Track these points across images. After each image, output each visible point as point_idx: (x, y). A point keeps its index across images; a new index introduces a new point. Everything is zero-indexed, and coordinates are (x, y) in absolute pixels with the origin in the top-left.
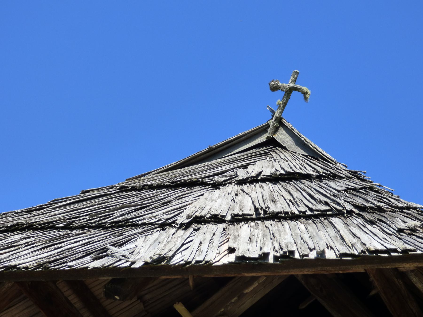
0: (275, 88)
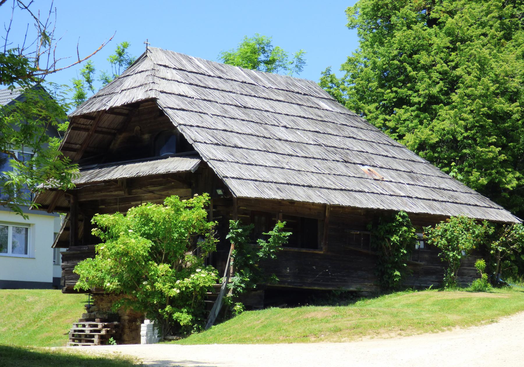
0: (144, 43)
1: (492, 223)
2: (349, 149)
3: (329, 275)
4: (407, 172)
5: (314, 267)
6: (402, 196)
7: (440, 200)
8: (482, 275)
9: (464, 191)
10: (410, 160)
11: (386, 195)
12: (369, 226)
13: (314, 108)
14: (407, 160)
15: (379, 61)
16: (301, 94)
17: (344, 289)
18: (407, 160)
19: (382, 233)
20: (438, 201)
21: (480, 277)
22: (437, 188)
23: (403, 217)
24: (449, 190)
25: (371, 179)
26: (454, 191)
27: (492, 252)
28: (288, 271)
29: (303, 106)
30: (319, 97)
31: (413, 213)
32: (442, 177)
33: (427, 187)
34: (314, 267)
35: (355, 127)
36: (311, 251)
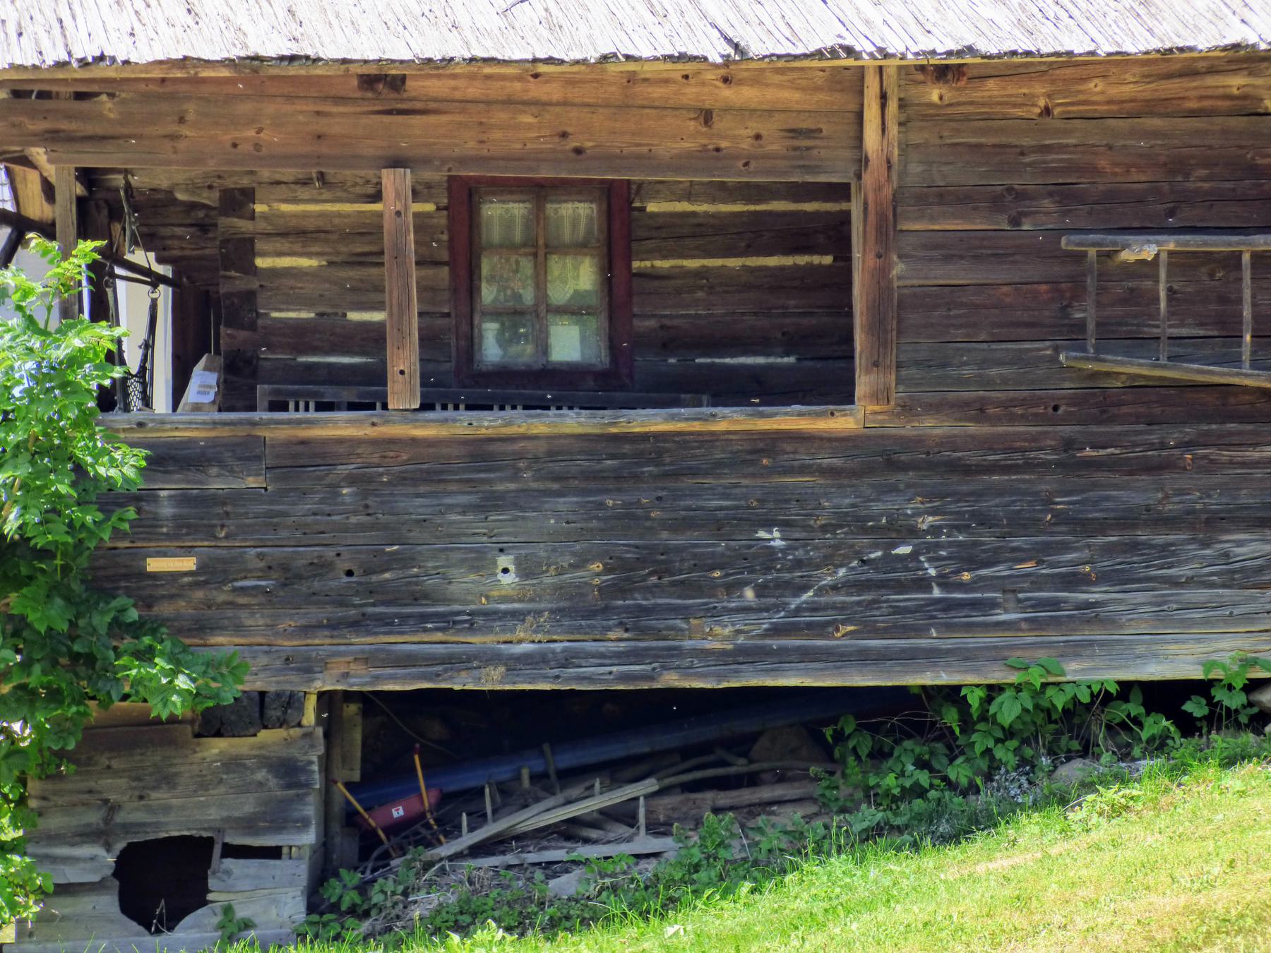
3: (923, 584)
28: (509, 579)
34: (775, 537)
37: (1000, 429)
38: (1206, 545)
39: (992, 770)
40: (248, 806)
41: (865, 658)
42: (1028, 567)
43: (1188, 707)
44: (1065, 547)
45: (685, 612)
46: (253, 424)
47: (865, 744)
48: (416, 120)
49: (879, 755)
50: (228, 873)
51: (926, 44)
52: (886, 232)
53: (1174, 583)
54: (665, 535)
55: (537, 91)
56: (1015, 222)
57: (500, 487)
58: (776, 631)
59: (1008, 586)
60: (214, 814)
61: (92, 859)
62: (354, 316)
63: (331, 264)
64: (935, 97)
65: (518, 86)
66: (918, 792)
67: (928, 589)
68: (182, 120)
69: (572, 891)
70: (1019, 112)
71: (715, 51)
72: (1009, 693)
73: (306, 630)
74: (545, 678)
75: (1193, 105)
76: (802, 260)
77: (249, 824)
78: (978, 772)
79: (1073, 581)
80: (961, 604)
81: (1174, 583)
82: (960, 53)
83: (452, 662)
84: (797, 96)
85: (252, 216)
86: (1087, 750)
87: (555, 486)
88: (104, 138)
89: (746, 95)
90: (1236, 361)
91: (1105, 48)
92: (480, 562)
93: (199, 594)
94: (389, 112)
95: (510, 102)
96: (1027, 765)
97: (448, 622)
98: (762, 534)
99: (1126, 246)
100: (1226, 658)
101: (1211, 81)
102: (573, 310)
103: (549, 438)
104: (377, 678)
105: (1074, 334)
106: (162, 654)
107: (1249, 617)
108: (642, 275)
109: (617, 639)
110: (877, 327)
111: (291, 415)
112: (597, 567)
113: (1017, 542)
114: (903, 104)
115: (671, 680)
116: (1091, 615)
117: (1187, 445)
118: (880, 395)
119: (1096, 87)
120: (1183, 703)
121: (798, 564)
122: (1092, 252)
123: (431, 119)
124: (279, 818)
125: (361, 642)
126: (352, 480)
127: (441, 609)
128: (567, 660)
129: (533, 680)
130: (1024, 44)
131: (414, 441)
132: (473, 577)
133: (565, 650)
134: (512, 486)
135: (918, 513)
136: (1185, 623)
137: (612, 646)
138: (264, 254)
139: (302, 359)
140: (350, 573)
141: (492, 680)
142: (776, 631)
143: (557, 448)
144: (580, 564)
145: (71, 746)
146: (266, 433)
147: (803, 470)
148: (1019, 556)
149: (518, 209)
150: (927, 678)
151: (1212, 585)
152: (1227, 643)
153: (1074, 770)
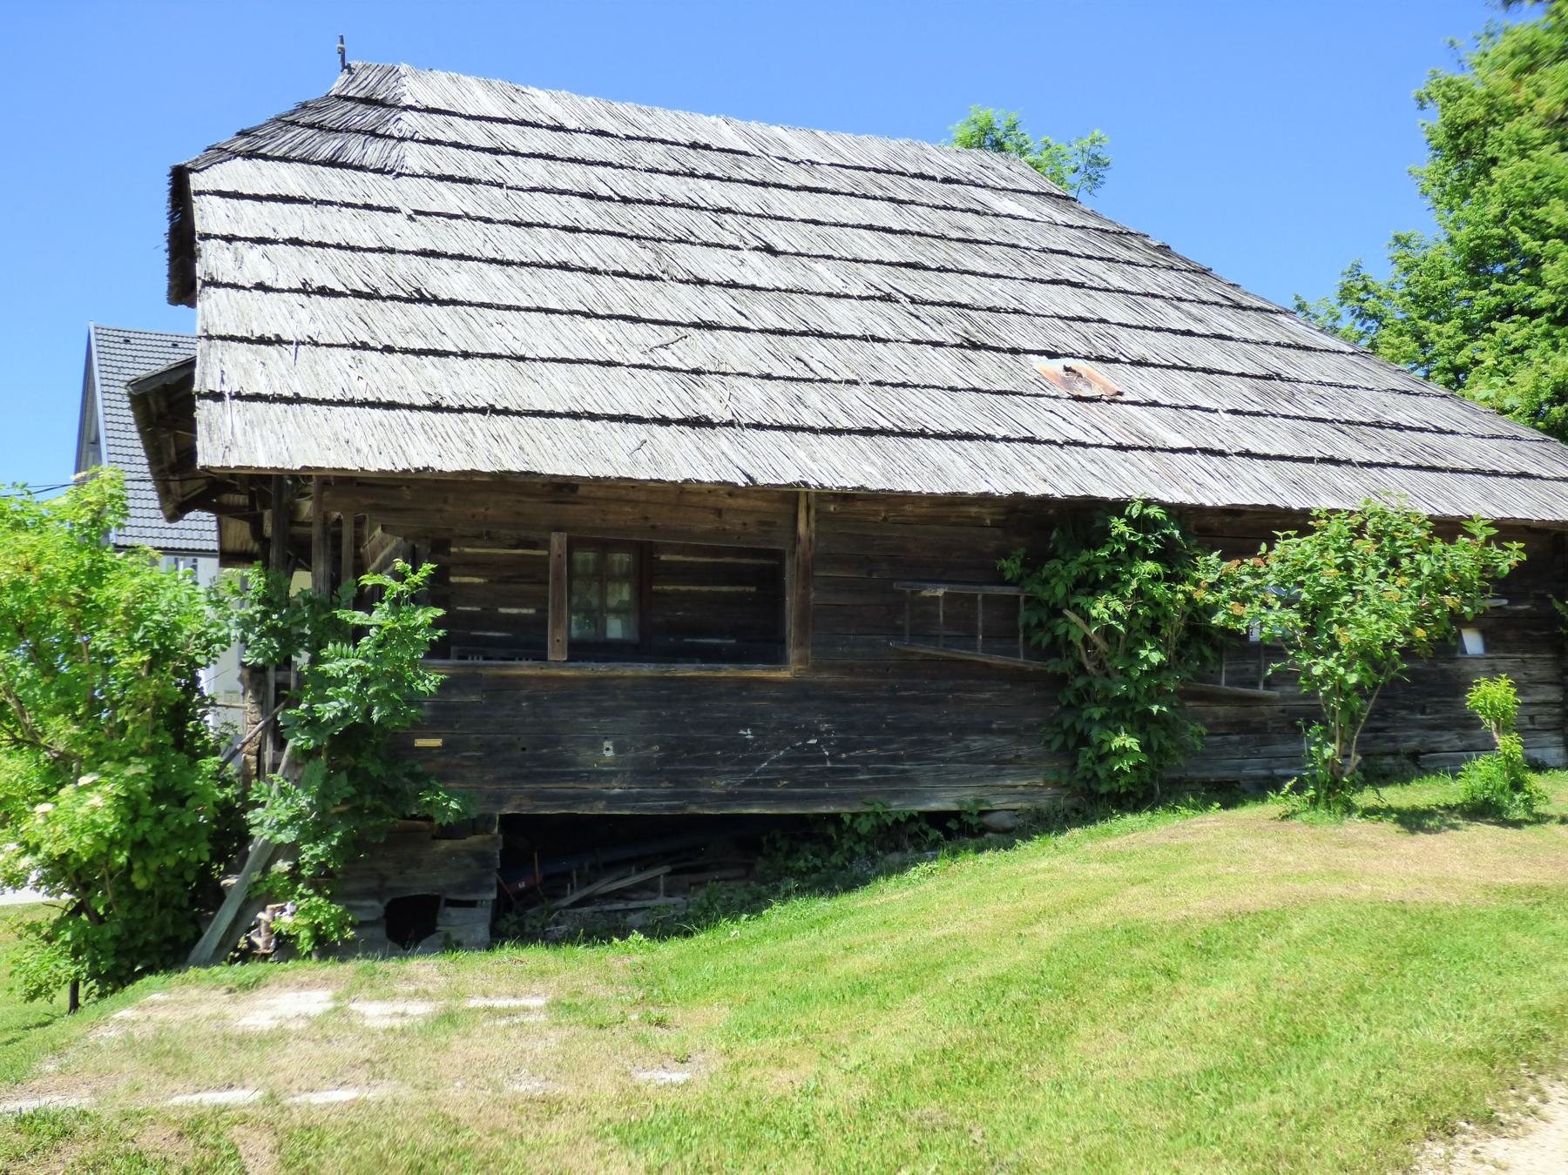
1: (1507, 530)
2: (1024, 313)
3: (823, 759)
4: (1256, 377)
5: (748, 734)
6: (1173, 451)
7: (1356, 459)
8: (1499, 741)
9: (1487, 432)
10: (1289, 346)
11: (1099, 446)
12: (1011, 567)
13: (962, 210)
14: (1278, 344)
15: (1463, 235)
16: (933, 178)
17: (900, 807)
18: (1278, 344)
19: (1060, 591)
20: (1348, 462)
21: (1490, 747)
22: (1369, 425)
23: (1143, 524)
24: (1421, 430)
25: (1056, 397)
26: (1440, 431)
27: (328, 892)
28: (609, 754)
29: (913, 207)
30: (1003, 189)
31: (1200, 509)
32: (1406, 392)
33: (1324, 421)
34: (748, 734)
35: (1101, 259)
36: (757, 672)
37: (861, 680)
38: (958, 742)
39: (852, 856)
40: (460, 878)
41: (793, 799)
42: (873, 751)
43: (949, 824)
44: (891, 742)
45: (702, 773)
46: (478, 666)
47: (784, 845)
48: (569, 507)
49: (791, 853)
50: (449, 915)
51: (843, 483)
52: (807, 576)
53: (943, 760)
54: (692, 731)
55: (632, 495)
56: (870, 574)
57: (606, 704)
58: (749, 783)
59: (865, 761)
60: (441, 882)
61: (372, 907)
62: (503, 610)
63: (491, 581)
64: (832, 509)
65: (624, 492)
66: (816, 869)
67: (825, 762)
68: (445, 501)
69: (208, 1013)
70: (872, 518)
71: (741, 481)
72: (862, 818)
73: (499, 780)
74: (627, 808)
75: (953, 520)
76: (740, 589)
77: (461, 888)
78: (846, 859)
79: (895, 759)
80: (841, 771)
81: (943, 760)
82: (858, 489)
83: (578, 799)
84: (765, 504)
85: (449, 554)
86: (898, 848)
87: (635, 704)
88: (402, 510)
89: (740, 502)
90: (974, 649)
91: (926, 490)
92: (595, 744)
93: (442, 760)
94: (556, 502)
95: (619, 500)
96: (872, 857)
97: (576, 776)
98: (742, 732)
99: (925, 589)
100: (969, 799)
101: (963, 509)
102: (617, 611)
103: (633, 678)
104: (537, 807)
105: (897, 633)
106: (441, 790)
107: (979, 779)
108: (657, 593)
109: (665, 787)
110: (802, 625)
111: (469, 662)
112: (656, 748)
113: (868, 738)
114: (817, 512)
115: (693, 809)
116: (905, 777)
117: (950, 691)
118: (801, 660)
119: (908, 508)
120: (946, 822)
121: (760, 748)
122: (908, 590)
123: (578, 507)
124: (476, 885)
125: (529, 787)
126: (527, 698)
127: (573, 769)
128: (639, 798)
129: (620, 809)
130: (889, 486)
131: (562, 678)
132: (590, 753)
133: (638, 793)
134: (612, 703)
135: (820, 722)
136: (949, 781)
137: (664, 791)
138: (455, 575)
139: (473, 633)
140: (524, 749)
141: (599, 809)
142: (749, 783)
143: (637, 682)
144: (649, 744)
145: (382, 840)
146: (483, 672)
147: (763, 698)
148: (869, 745)
149: (591, 556)
150: (823, 810)
151: (961, 762)
152: (969, 792)
153: (895, 857)
